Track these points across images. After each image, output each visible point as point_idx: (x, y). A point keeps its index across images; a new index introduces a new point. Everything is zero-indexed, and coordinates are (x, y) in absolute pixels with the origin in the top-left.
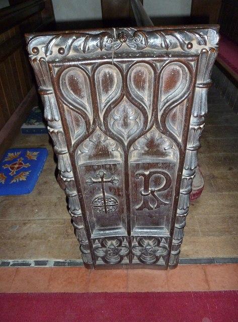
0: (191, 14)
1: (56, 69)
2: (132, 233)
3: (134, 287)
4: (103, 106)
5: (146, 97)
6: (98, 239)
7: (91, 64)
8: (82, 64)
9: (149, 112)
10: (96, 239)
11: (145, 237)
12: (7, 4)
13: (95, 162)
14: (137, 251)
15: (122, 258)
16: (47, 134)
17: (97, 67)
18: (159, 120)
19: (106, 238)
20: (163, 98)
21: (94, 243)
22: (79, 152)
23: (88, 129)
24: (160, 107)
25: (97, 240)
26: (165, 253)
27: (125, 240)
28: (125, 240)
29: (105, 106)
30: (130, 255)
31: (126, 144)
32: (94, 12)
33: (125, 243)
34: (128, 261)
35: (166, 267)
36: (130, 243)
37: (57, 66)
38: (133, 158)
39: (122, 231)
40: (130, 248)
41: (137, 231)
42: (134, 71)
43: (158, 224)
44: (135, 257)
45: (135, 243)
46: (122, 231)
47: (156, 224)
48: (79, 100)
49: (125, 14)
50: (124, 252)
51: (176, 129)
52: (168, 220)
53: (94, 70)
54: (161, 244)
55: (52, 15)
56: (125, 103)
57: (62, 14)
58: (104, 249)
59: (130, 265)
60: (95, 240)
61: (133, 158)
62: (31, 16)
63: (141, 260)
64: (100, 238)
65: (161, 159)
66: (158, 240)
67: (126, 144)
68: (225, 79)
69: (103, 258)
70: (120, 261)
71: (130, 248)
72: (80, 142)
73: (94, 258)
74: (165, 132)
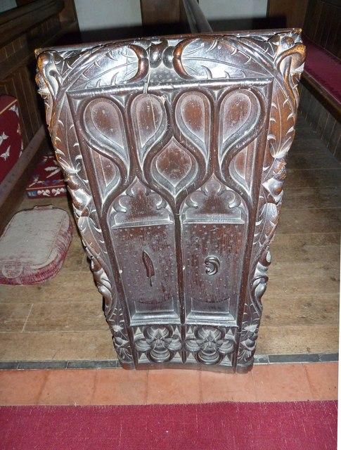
0: (268, 13)
1: (78, 102)
2: (131, 321)
3: (190, 397)
4: (223, 147)
5: (200, 139)
6: (139, 326)
7: (124, 93)
8: (207, 87)
9: (207, 158)
10: (137, 326)
11: (156, 326)
12: (15, 5)
13: (136, 222)
14: (193, 346)
15: (172, 354)
16: (54, 255)
17: (134, 97)
18: (142, 167)
19: (150, 325)
20: (224, 139)
21: (227, 332)
22: (113, 210)
23: (123, 181)
24: (220, 151)
25: (138, 328)
26: (230, 348)
27: (177, 329)
28: (177, 329)
29: (223, 152)
30: (184, 352)
31: (175, 197)
32: (132, 17)
33: (230, 335)
34: (180, 360)
35: (234, 368)
36: (183, 332)
37: (78, 98)
38: (186, 219)
39: (174, 318)
40: (184, 340)
41: (193, 319)
42: (182, 110)
43: (221, 309)
44: (191, 354)
45: (190, 334)
46: (174, 318)
47: (214, 306)
48: (110, 141)
49: (174, 16)
50: (175, 345)
51: (243, 179)
52: (233, 303)
53: (176, 100)
54: (227, 336)
55: (73, 17)
56: (173, 144)
57: (87, 20)
58: (198, 341)
59: (184, 365)
60: (135, 327)
61: (186, 219)
62: (46, 20)
63: (151, 359)
64: (195, 325)
65: (149, 222)
66: (222, 331)
67: (175, 197)
68: (317, 107)
69: (148, 354)
70: (170, 358)
71: (184, 340)
72: (113, 199)
73: (135, 354)
74: (229, 182)
